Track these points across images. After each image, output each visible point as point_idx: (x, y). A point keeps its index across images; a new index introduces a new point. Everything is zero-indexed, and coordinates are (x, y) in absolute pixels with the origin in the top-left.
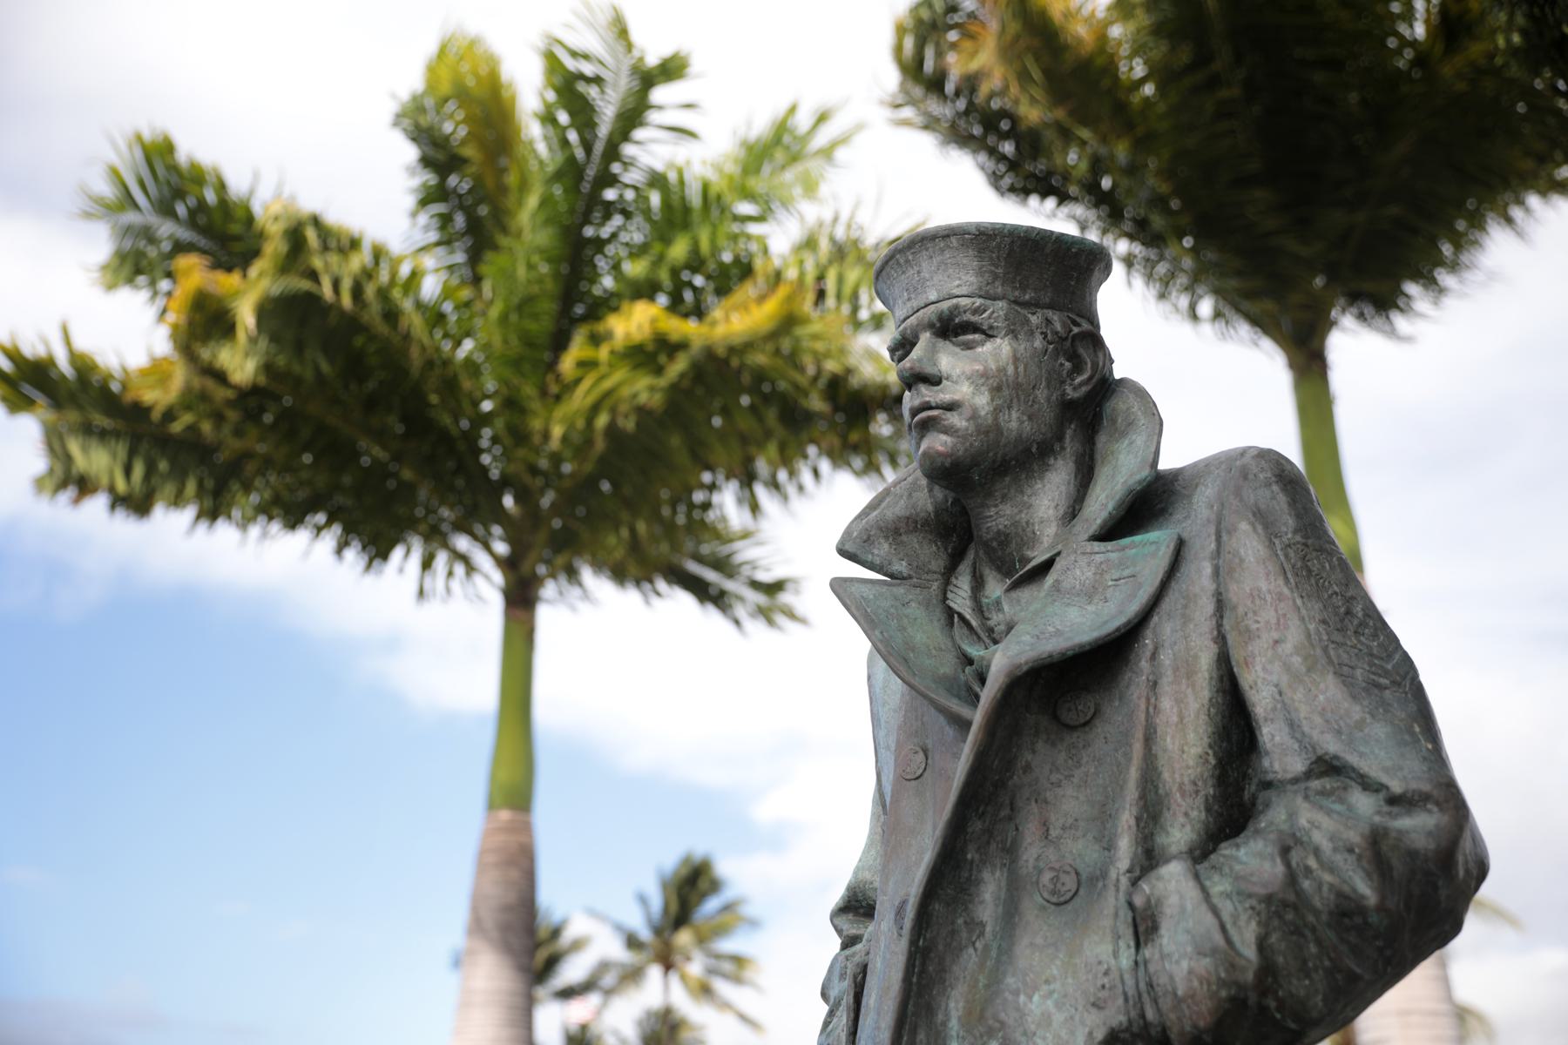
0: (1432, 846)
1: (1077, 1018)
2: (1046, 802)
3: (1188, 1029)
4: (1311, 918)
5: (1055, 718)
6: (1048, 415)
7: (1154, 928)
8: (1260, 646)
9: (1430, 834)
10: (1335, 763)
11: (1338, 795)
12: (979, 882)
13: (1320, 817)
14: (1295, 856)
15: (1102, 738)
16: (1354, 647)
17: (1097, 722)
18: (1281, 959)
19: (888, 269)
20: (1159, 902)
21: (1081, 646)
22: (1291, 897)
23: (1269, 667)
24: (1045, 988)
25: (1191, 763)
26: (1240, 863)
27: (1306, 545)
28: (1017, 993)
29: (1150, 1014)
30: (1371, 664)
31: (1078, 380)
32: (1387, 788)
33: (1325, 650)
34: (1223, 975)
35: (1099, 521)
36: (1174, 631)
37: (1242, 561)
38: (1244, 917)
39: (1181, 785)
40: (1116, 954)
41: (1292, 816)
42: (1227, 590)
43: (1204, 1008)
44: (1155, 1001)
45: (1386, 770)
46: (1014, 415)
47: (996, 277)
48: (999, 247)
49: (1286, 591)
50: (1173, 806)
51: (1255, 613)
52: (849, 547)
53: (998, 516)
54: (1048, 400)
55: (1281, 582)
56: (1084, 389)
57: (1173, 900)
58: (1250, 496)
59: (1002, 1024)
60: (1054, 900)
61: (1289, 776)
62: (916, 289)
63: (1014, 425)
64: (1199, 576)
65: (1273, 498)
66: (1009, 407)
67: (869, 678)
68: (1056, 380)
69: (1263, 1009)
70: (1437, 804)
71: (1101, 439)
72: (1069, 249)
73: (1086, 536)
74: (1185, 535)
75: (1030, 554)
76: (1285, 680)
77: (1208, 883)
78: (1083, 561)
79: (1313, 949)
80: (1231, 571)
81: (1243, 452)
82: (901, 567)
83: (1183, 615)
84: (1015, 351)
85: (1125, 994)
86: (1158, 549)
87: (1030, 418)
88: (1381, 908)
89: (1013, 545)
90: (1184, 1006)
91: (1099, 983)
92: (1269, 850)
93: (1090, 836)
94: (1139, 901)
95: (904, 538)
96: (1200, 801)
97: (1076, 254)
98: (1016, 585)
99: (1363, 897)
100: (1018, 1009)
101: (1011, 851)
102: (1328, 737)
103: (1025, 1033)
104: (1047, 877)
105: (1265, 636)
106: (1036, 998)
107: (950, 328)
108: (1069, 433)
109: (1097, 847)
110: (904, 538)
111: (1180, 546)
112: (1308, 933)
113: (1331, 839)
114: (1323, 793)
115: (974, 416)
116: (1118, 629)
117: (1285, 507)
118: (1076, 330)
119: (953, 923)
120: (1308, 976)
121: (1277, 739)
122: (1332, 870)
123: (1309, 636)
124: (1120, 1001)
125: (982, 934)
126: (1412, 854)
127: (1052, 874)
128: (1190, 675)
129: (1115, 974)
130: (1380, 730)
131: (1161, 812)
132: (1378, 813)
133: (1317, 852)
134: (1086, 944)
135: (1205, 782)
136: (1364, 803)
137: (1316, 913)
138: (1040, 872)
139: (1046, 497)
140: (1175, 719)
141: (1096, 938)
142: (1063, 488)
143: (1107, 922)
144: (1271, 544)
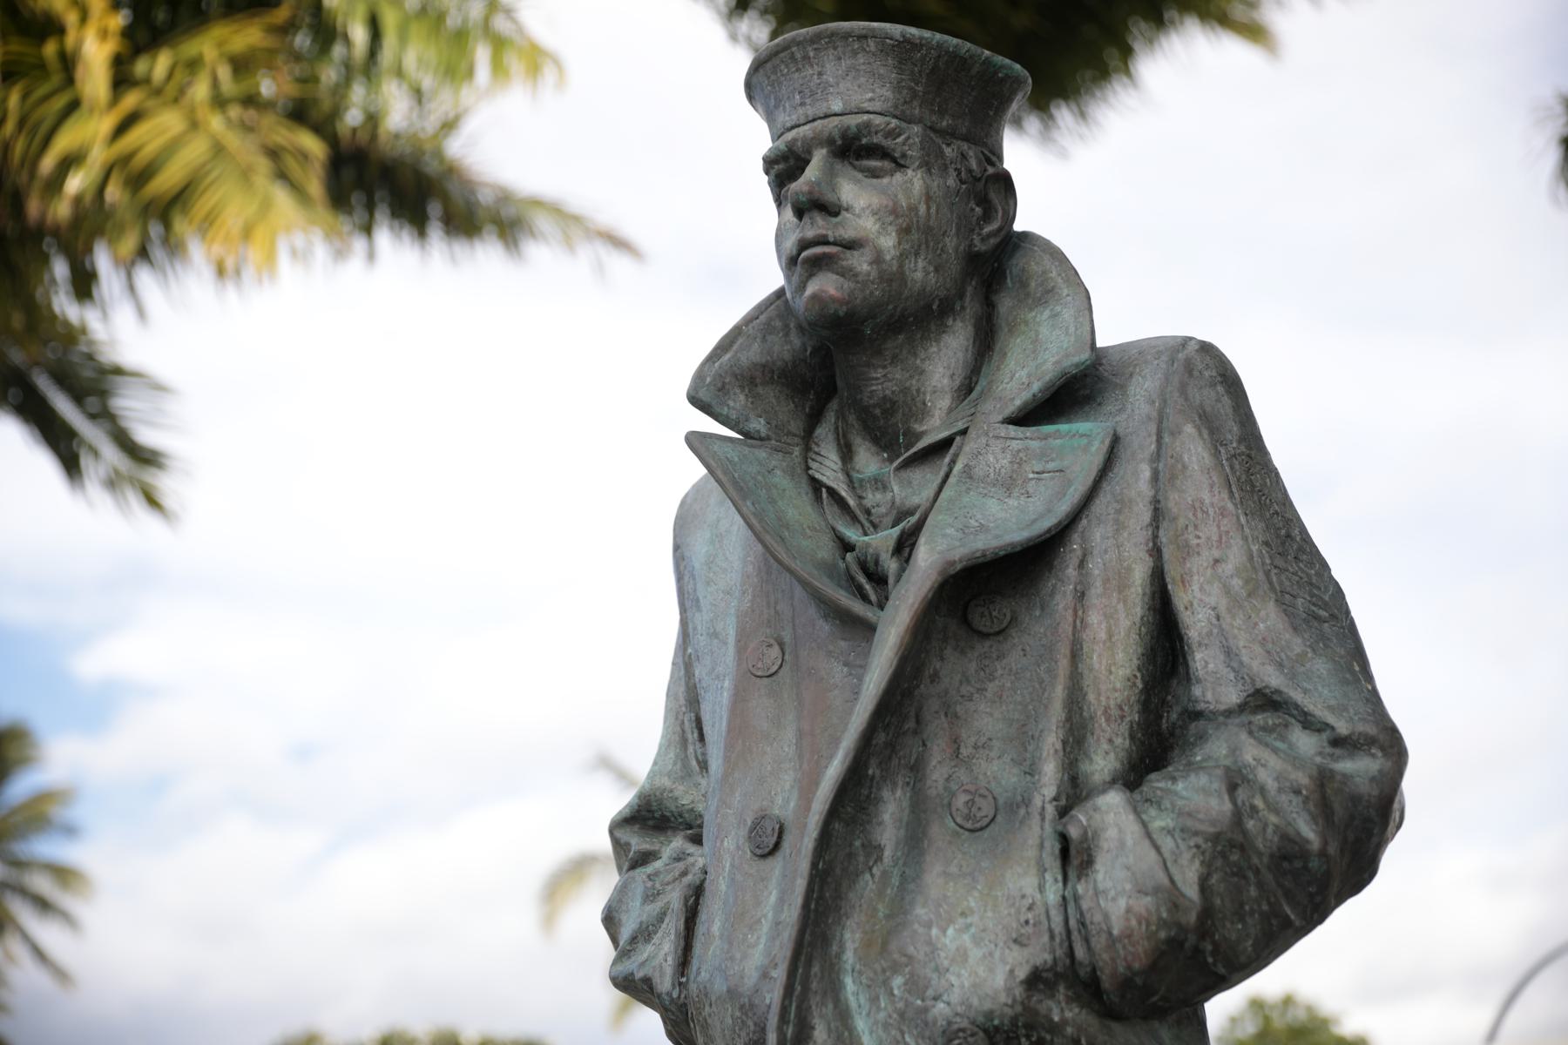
0: (1375, 792)
1: (997, 954)
2: (956, 716)
3: (1121, 969)
4: (1255, 860)
5: (965, 621)
6: (954, 267)
7: (1088, 863)
8: (1199, 564)
9: (1373, 779)
10: (1276, 697)
11: (1280, 731)
12: (878, 800)
13: (1266, 755)
14: (1241, 794)
15: (1017, 655)
16: (1295, 574)
17: (1013, 632)
18: (1218, 902)
19: (776, 61)
20: (1096, 834)
21: (1012, 545)
22: (1240, 838)
23: (1207, 587)
24: (961, 921)
25: (1118, 685)
26: (1182, 798)
27: (1249, 456)
28: (929, 925)
29: (1080, 952)
30: (1312, 595)
31: (987, 229)
32: (1333, 728)
33: (1267, 574)
34: (1165, 915)
35: (1018, 402)
36: (1104, 538)
37: (1185, 467)
38: (1187, 856)
39: (1106, 711)
40: (1041, 888)
41: (1234, 751)
42: (1166, 499)
43: (1140, 950)
44: (1087, 940)
45: (1330, 708)
46: (921, 264)
47: (914, 95)
48: (923, 58)
49: (1230, 506)
50: (1097, 732)
51: (1196, 527)
52: (703, 395)
53: (882, 381)
54: (956, 250)
55: (1225, 495)
56: (993, 241)
57: (1112, 833)
58: (1196, 396)
59: (910, 958)
60: (969, 825)
61: (1222, 707)
62: (813, 94)
63: (919, 275)
64: (1136, 478)
65: (1218, 400)
66: (917, 254)
67: (677, 548)
68: (966, 228)
69: (1197, 951)
70: (1382, 749)
71: (1005, 304)
72: (996, 73)
73: (1000, 418)
74: (1120, 431)
75: (918, 428)
76: (1223, 604)
77: (1144, 817)
78: (997, 446)
79: (1253, 891)
80: (1173, 478)
81: (1187, 340)
82: (758, 425)
83: (1117, 521)
84: (928, 188)
85: (1051, 931)
86: (1090, 443)
87: (936, 270)
88: (1323, 853)
89: (899, 415)
90: (1119, 946)
91: (1022, 919)
92: (1216, 785)
93: (1007, 758)
94: (1074, 832)
95: (760, 390)
96: (1124, 728)
97: (1002, 80)
98: (909, 463)
99: (1307, 841)
100: (929, 943)
101: (917, 769)
102: (1270, 669)
103: (937, 969)
104: (962, 799)
105: (1205, 553)
106: (950, 931)
107: (852, 149)
108: (970, 290)
109: (1015, 771)
110: (760, 390)
111: (1116, 441)
112: (1250, 875)
113: (1277, 779)
114: (1264, 729)
115: (878, 260)
116: (1049, 530)
117: (1230, 411)
118: (991, 170)
119: (851, 845)
120: (1242, 919)
121: (1211, 666)
122: (1276, 810)
123: (1251, 558)
124: (1046, 938)
125: (880, 859)
126: (1355, 799)
127: (968, 797)
128: (1122, 587)
129: (1040, 910)
130: (1321, 666)
131: (1084, 737)
132: (1320, 754)
133: (1263, 790)
134: (1008, 875)
135: (1131, 706)
136: (1306, 743)
137: (1260, 854)
138: (953, 795)
139: (944, 360)
140: (1103, 635)
141: (1020, 870)
142: (960, 355)
143: (1031, 853)
144: (1216, 454)
